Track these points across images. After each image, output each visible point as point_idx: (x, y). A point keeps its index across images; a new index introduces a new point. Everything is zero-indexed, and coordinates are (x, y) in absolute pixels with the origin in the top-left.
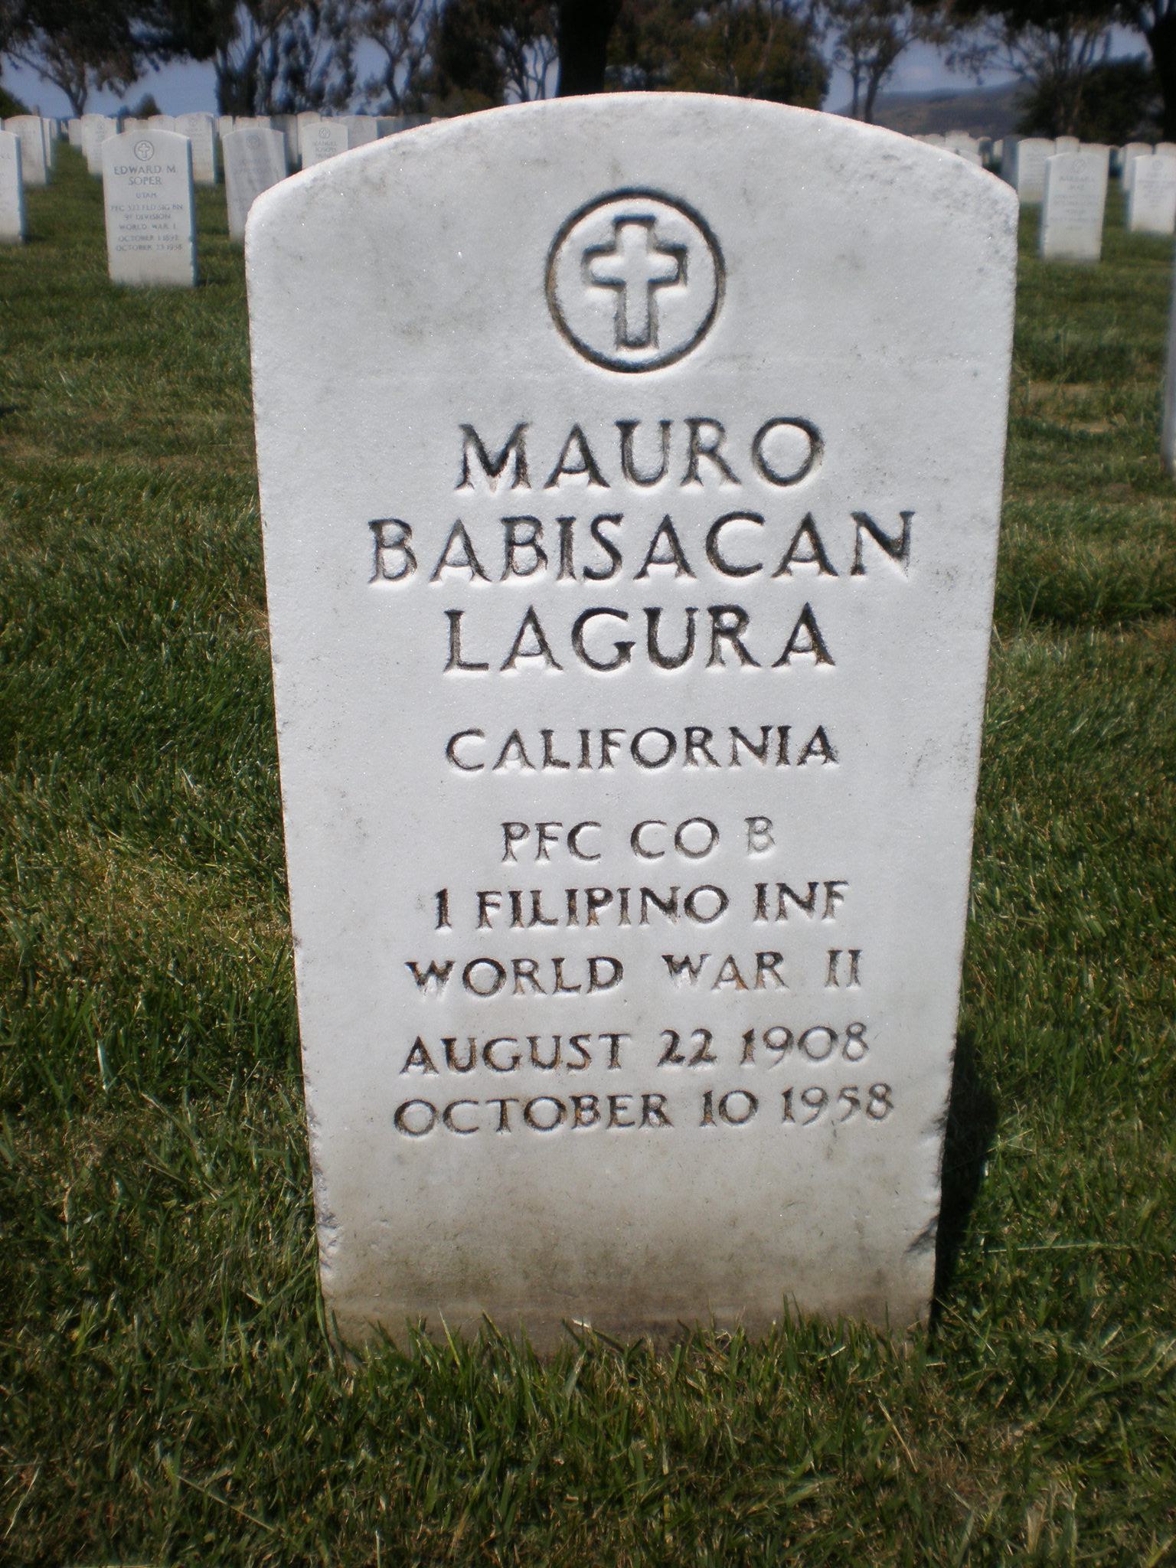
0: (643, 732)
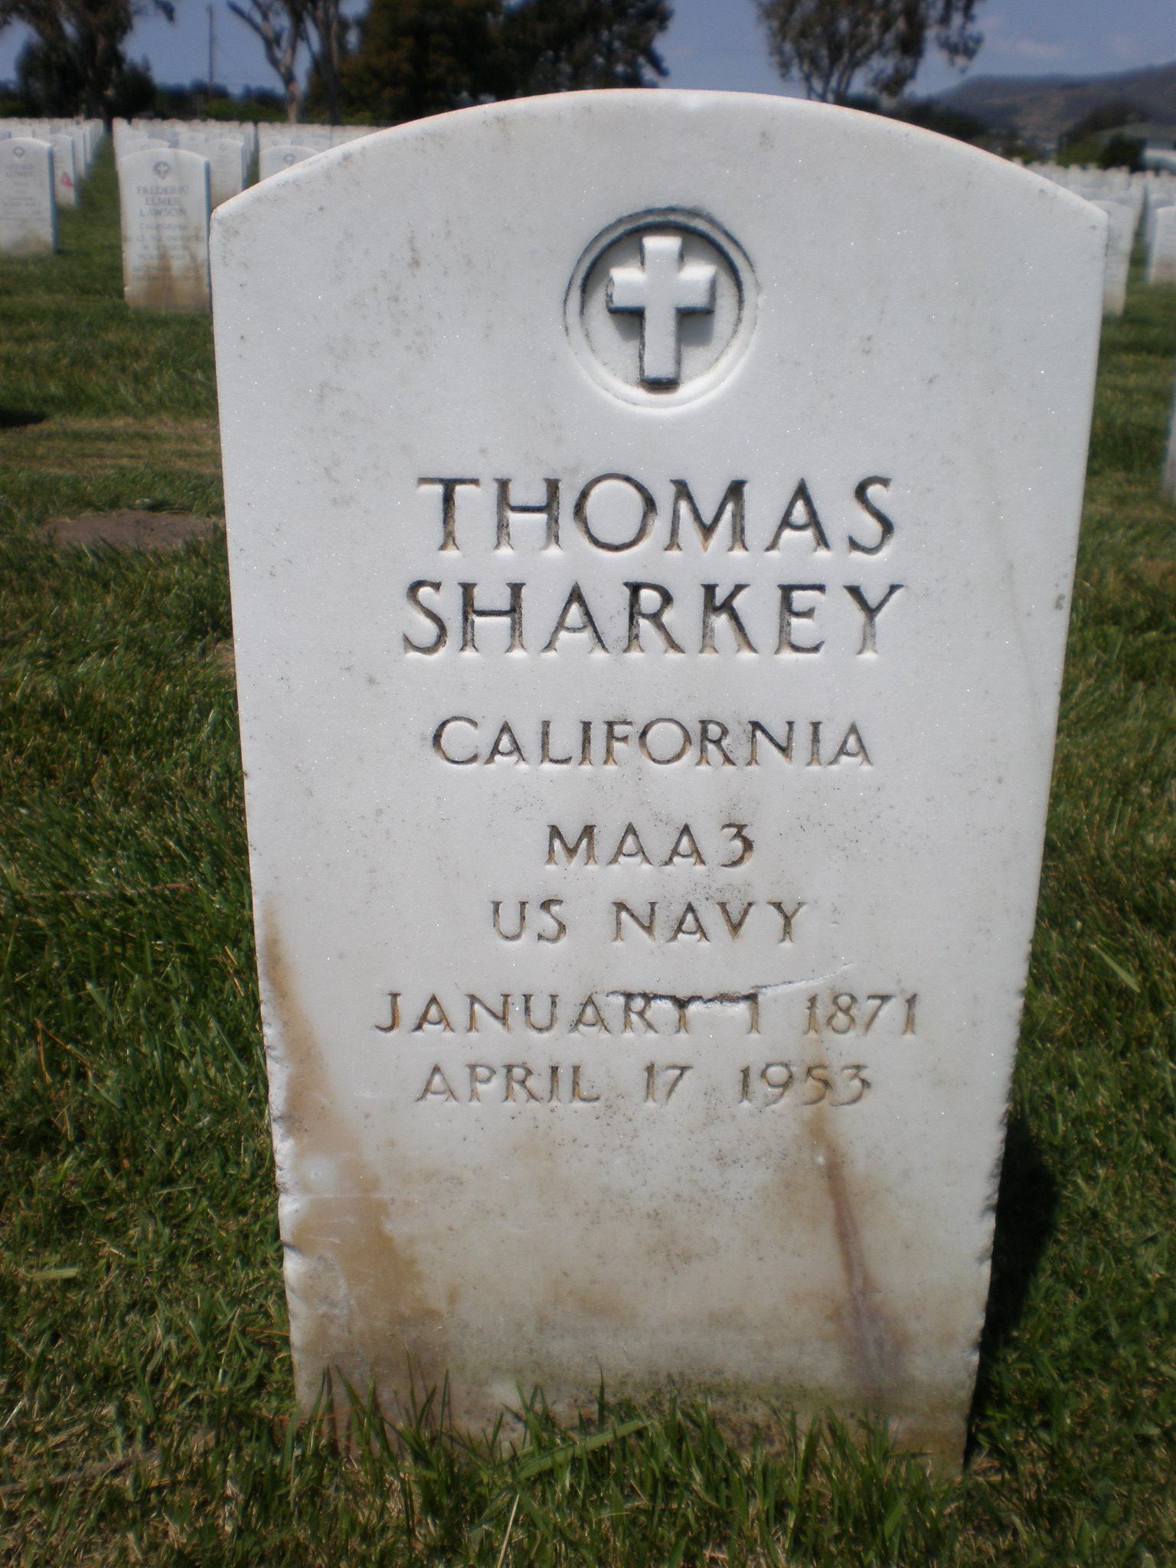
0: (658, 720)
